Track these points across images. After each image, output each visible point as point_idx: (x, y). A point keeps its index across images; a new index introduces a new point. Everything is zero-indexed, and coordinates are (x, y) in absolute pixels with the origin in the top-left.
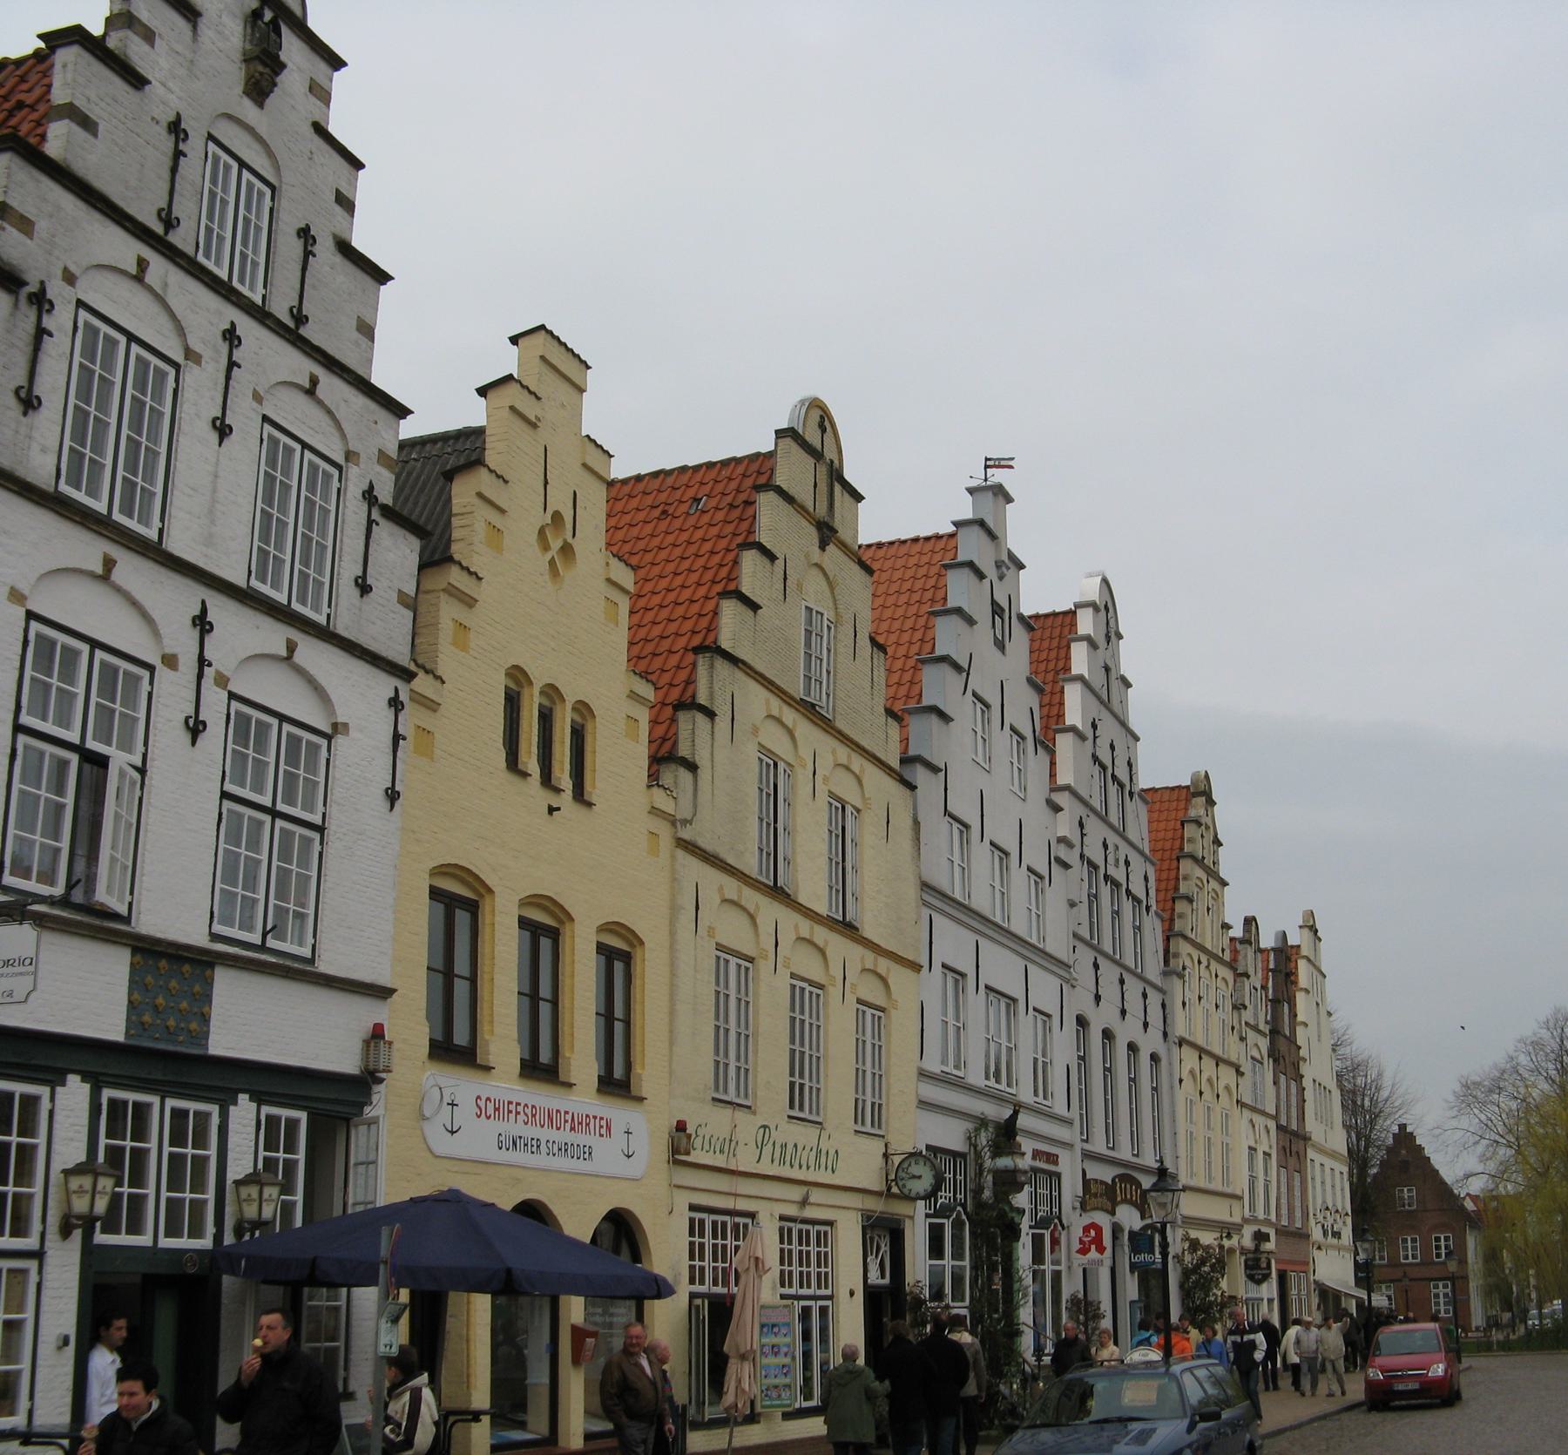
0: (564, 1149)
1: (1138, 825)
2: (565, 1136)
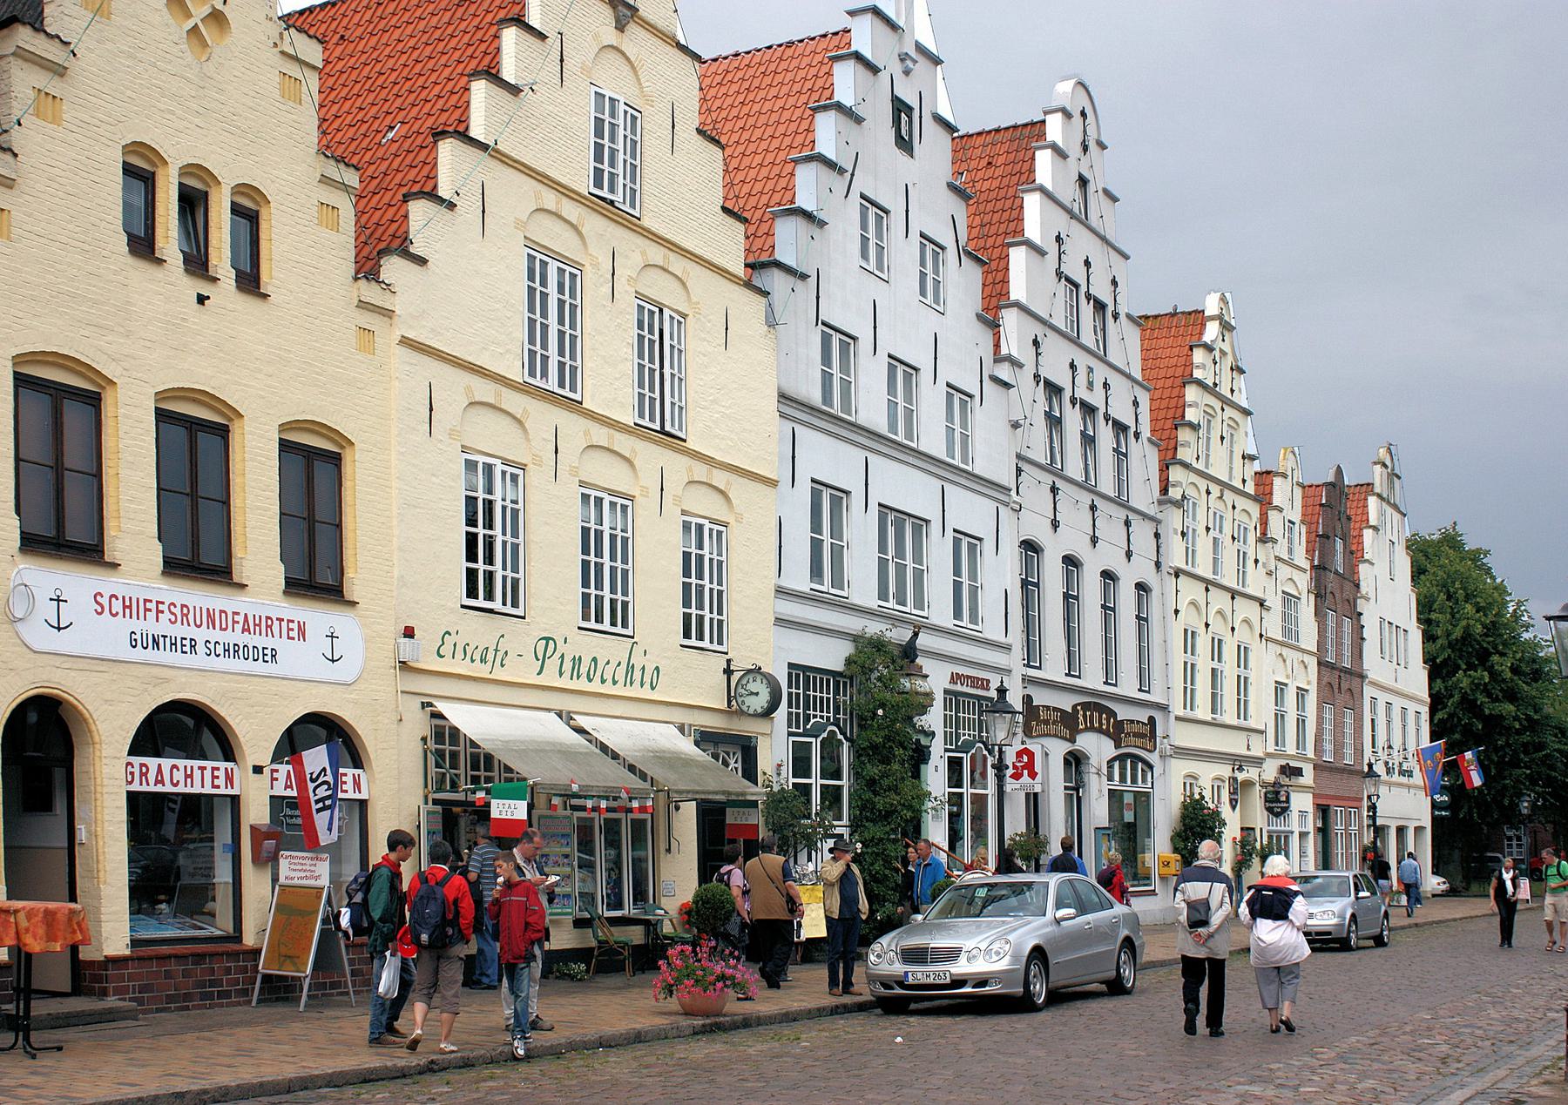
0: (234, 651)
1: (1126, 347)
2: (236, 637)
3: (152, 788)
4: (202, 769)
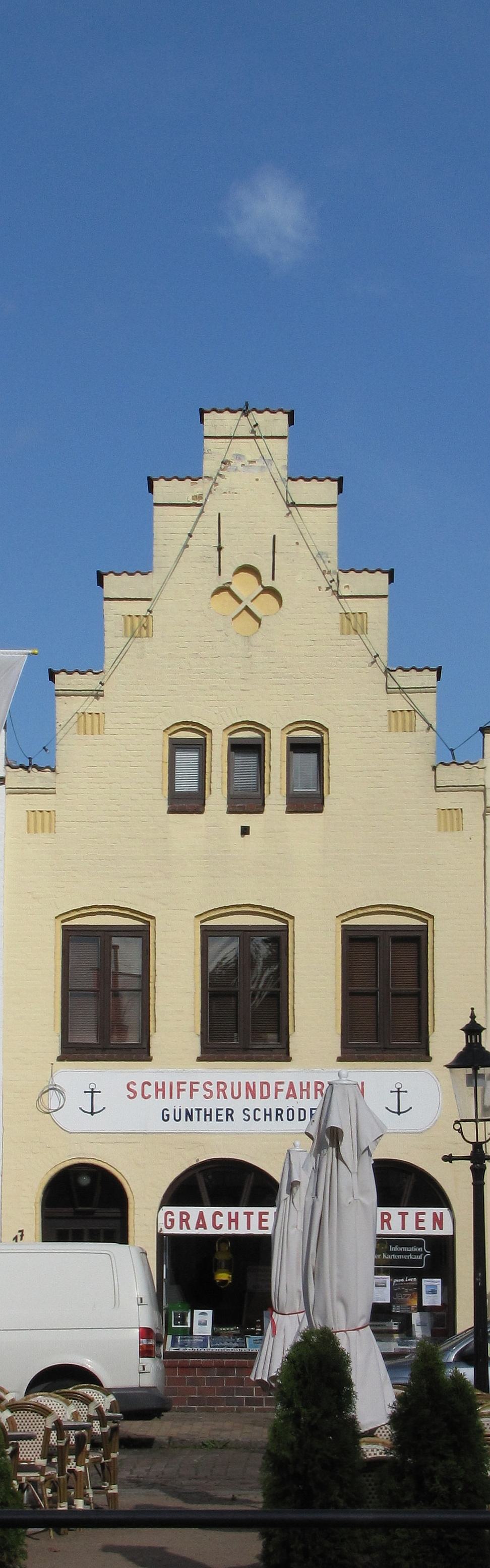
3: (193, 1231)
4: (249, 1214)
